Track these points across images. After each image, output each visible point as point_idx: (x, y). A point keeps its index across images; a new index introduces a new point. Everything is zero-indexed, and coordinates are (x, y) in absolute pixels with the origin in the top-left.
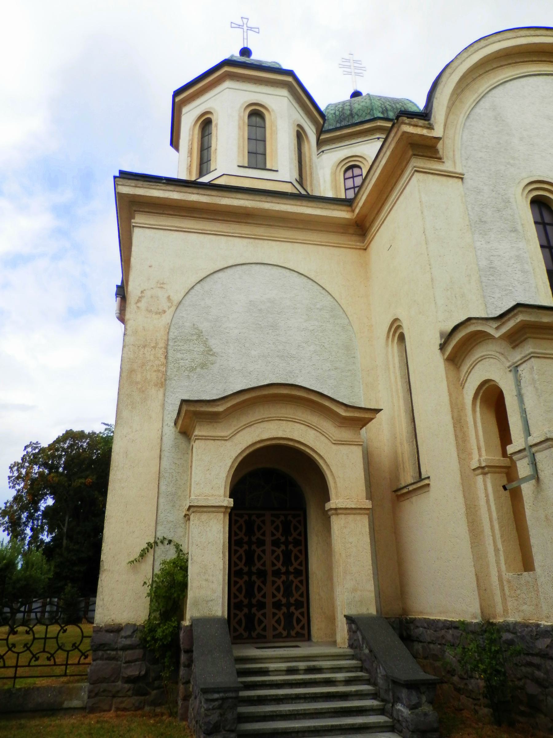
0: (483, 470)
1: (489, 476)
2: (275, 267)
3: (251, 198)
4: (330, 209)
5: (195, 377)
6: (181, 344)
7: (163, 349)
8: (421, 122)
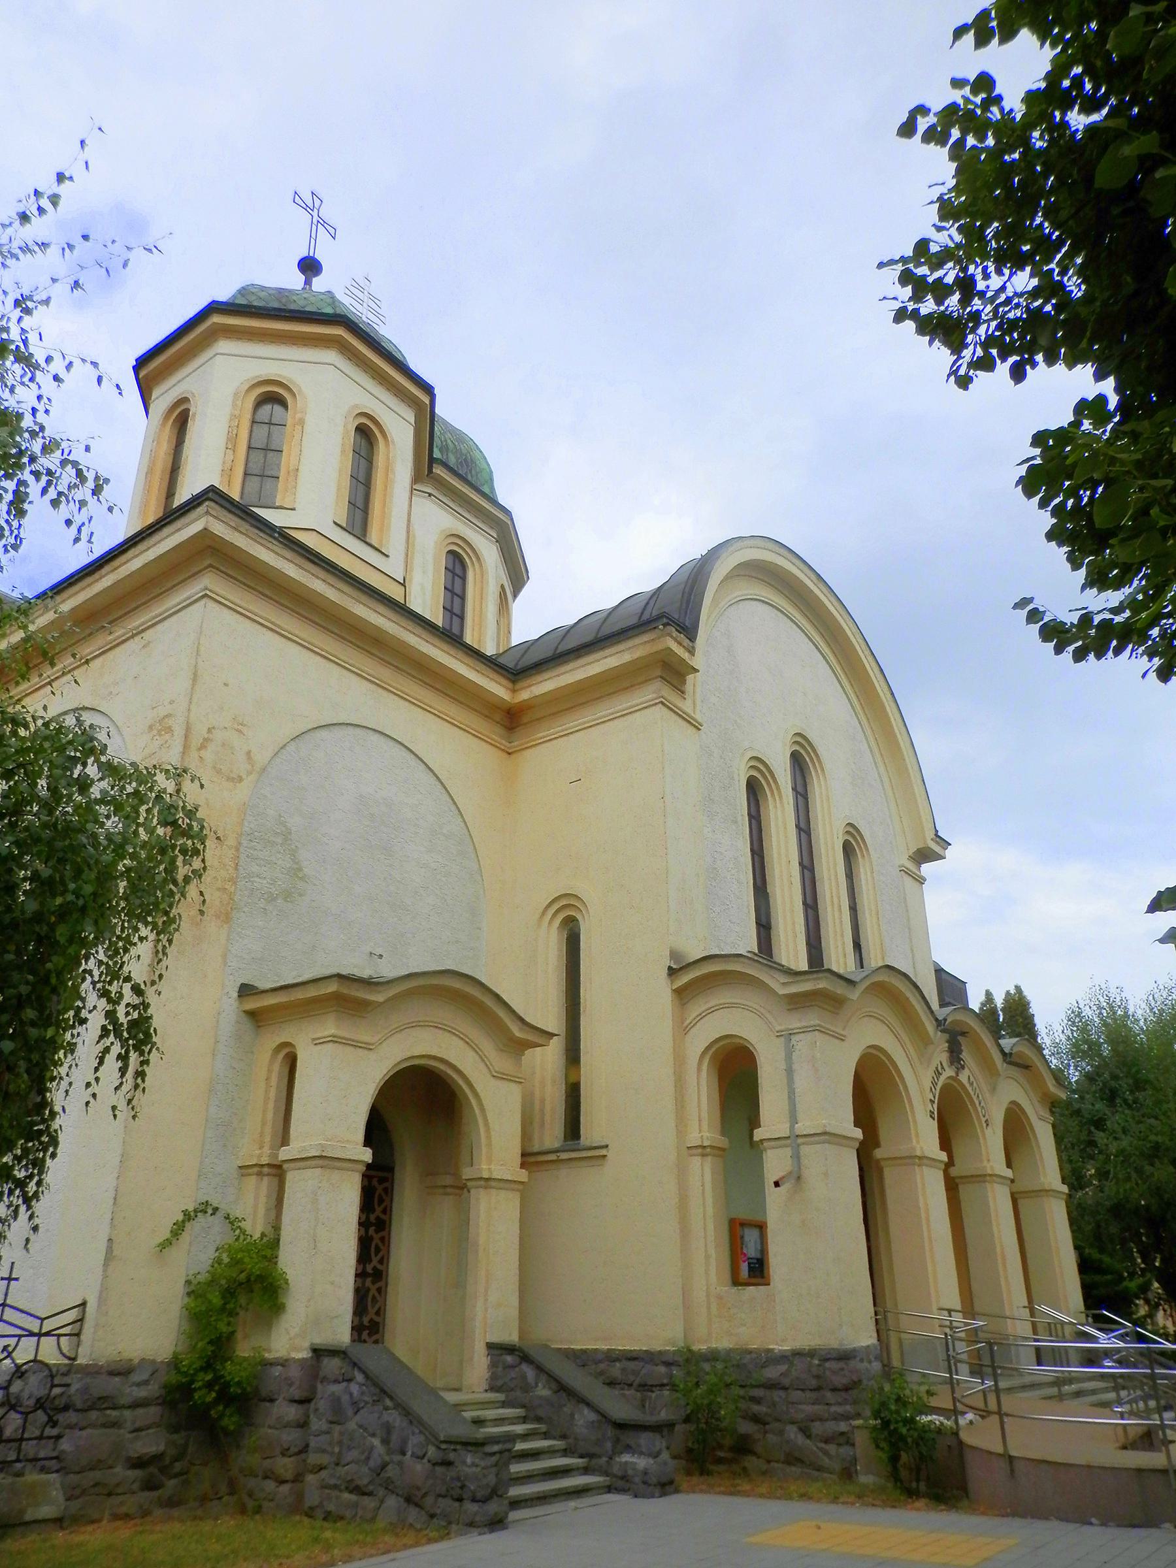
0: (702, 1150)
1: (709, 1158)
5: (274, 914)
6: (259, 847)
7: (233, 851)
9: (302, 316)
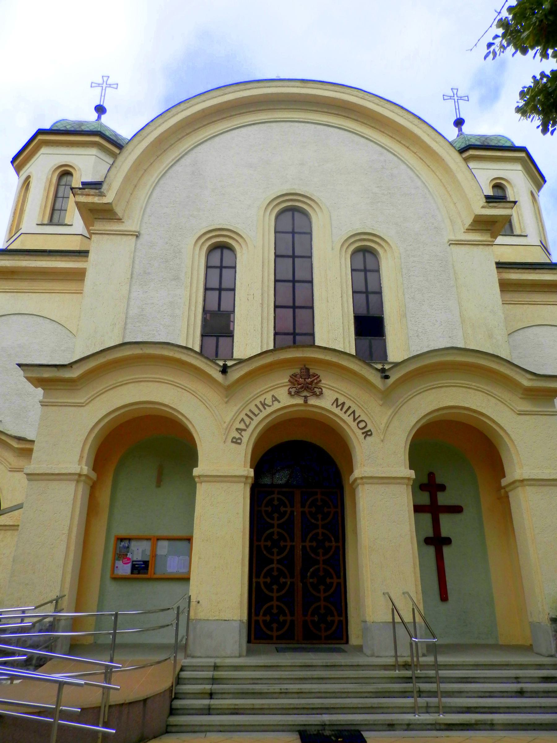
2: (32, 316)
3: (11, 259)
4: (82, 261)
8: (92, 192)
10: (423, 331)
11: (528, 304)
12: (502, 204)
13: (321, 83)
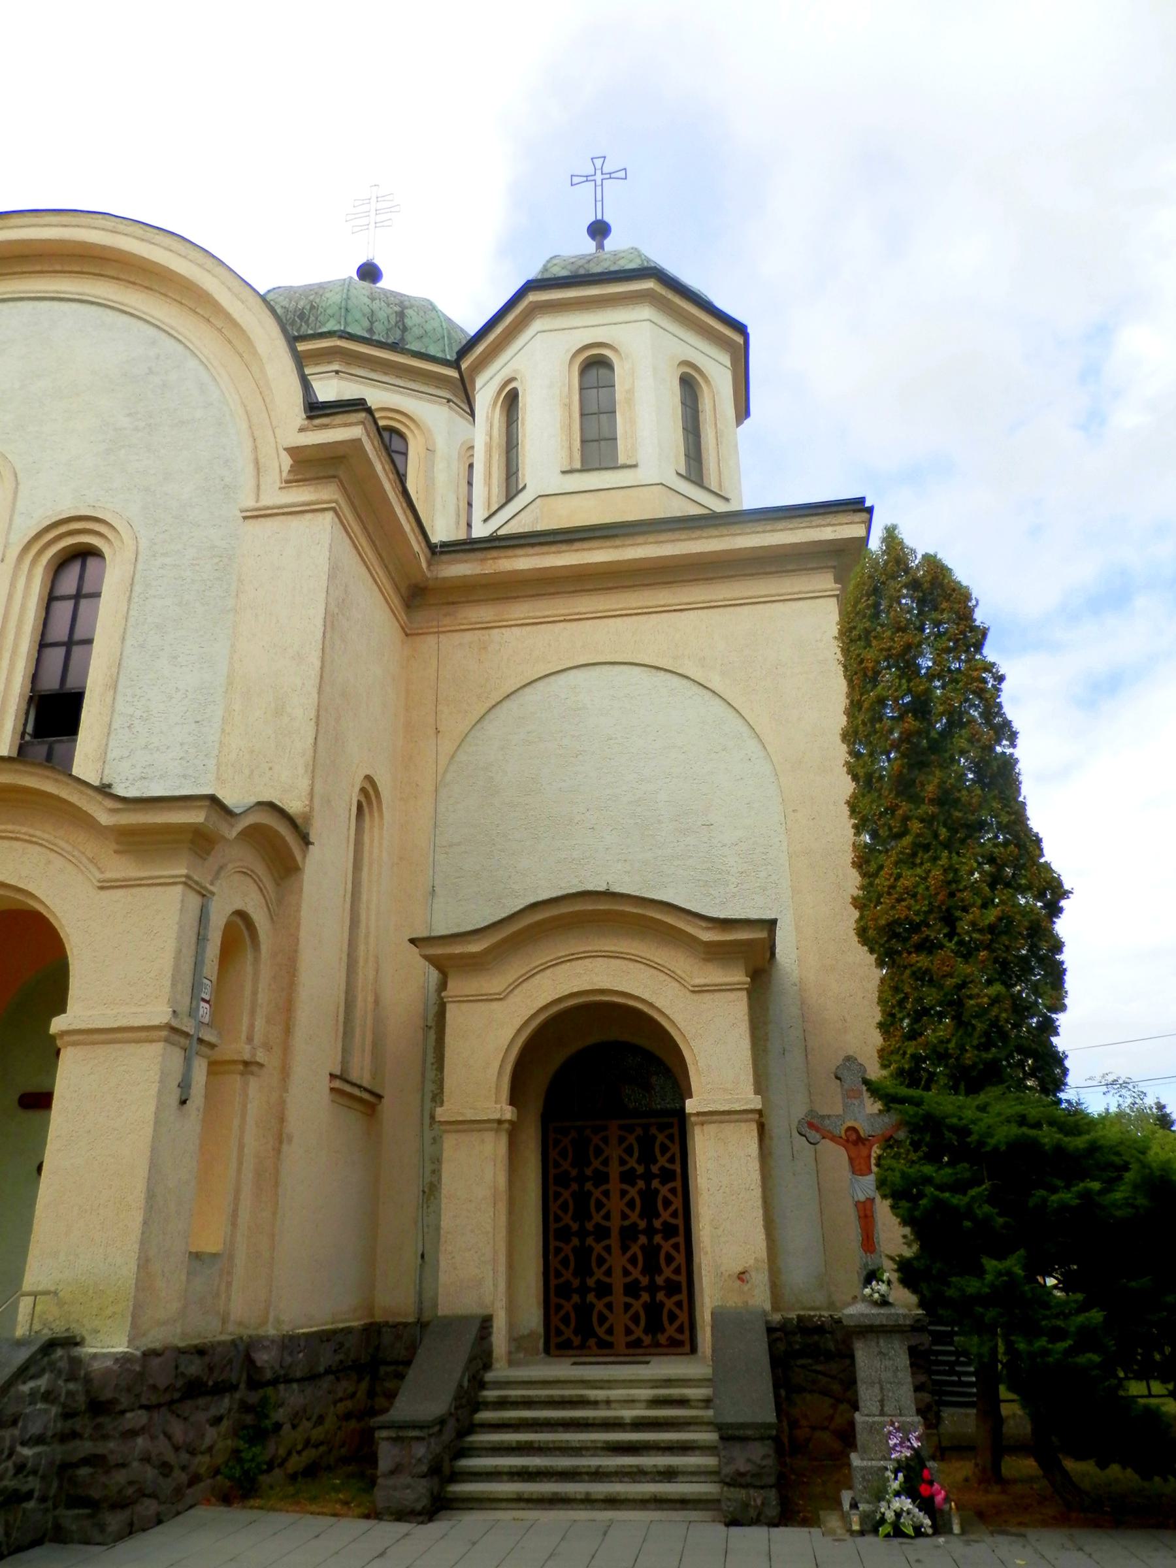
9: (591, 279)
10: (145, 715)
11: (565, 620)
12: (340, 416)
13: (34, 214)
